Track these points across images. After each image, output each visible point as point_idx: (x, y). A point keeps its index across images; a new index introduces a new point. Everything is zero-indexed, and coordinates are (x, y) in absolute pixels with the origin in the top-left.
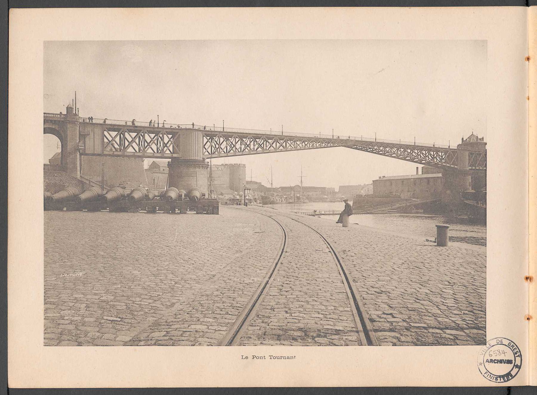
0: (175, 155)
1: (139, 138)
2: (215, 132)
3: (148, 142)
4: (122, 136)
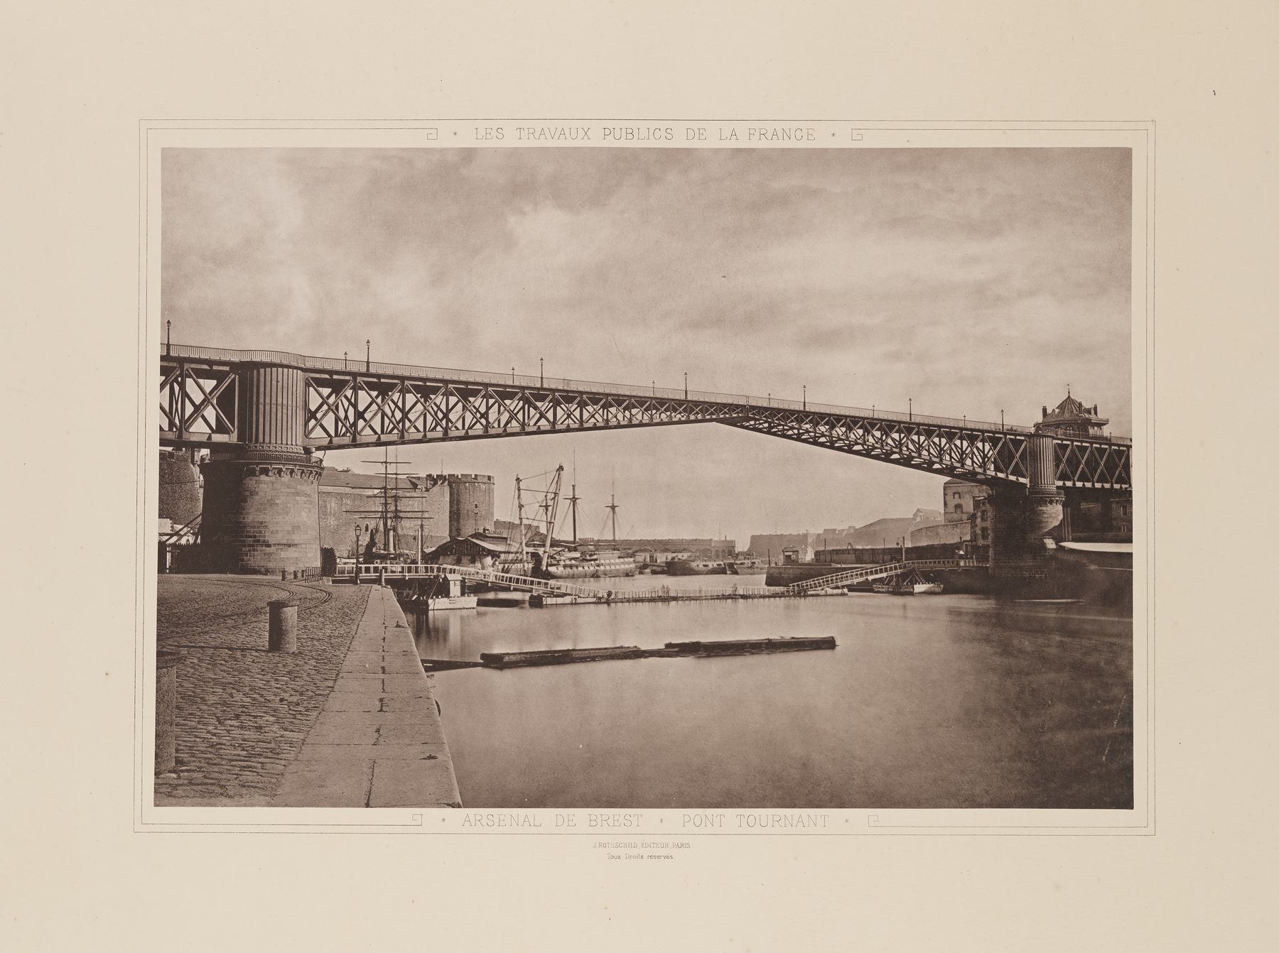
0: (217, 438)
3: (197, 404)
4: (176, 388)
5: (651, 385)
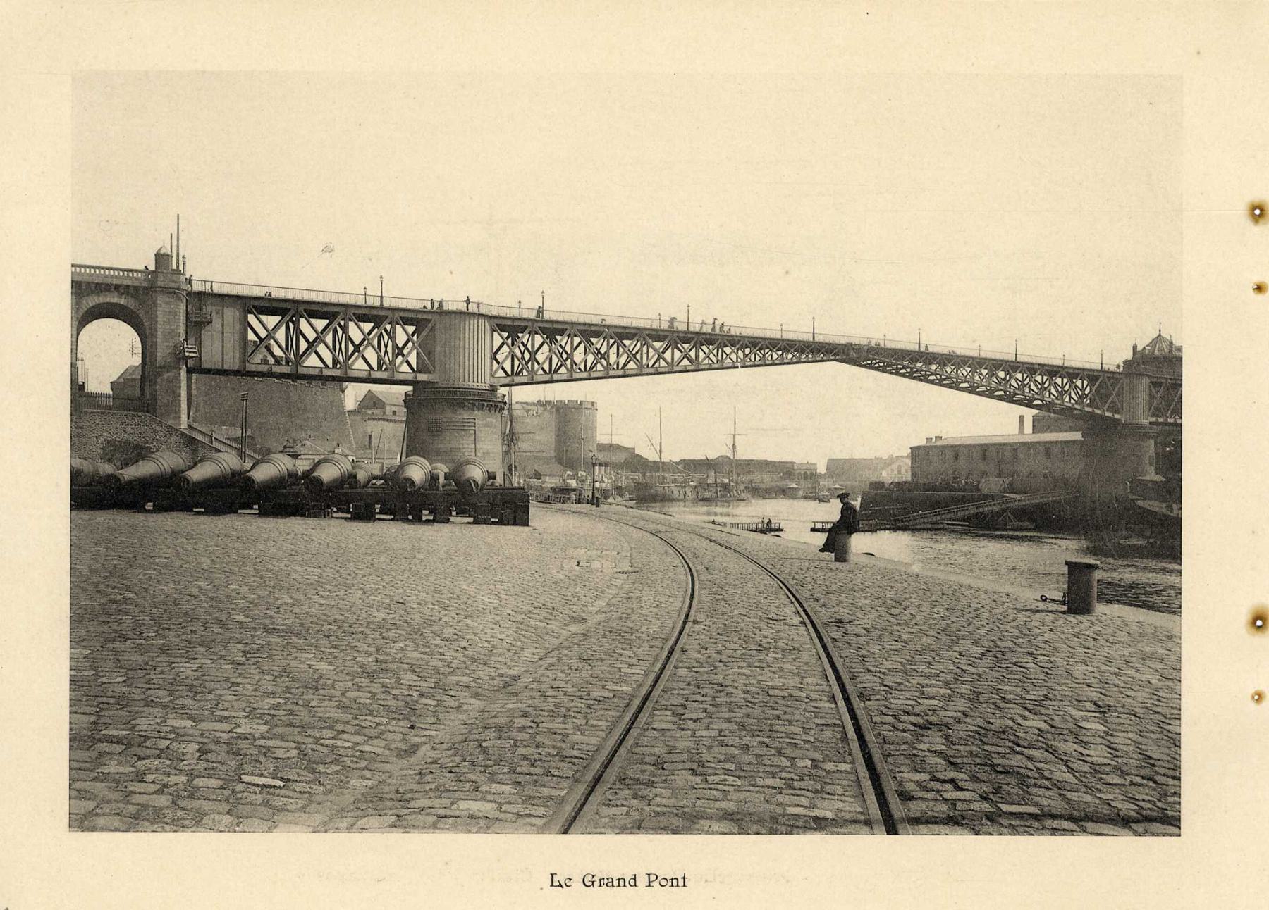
0: (422, 377)
1: (335, 331)
2: (381, 307)
3: (357, 343)
4: (291, 326)
5: (883, 337)
